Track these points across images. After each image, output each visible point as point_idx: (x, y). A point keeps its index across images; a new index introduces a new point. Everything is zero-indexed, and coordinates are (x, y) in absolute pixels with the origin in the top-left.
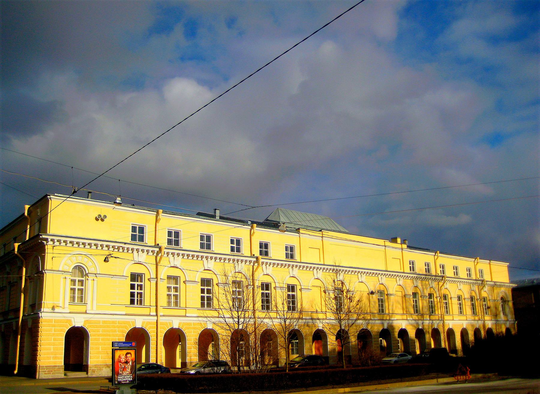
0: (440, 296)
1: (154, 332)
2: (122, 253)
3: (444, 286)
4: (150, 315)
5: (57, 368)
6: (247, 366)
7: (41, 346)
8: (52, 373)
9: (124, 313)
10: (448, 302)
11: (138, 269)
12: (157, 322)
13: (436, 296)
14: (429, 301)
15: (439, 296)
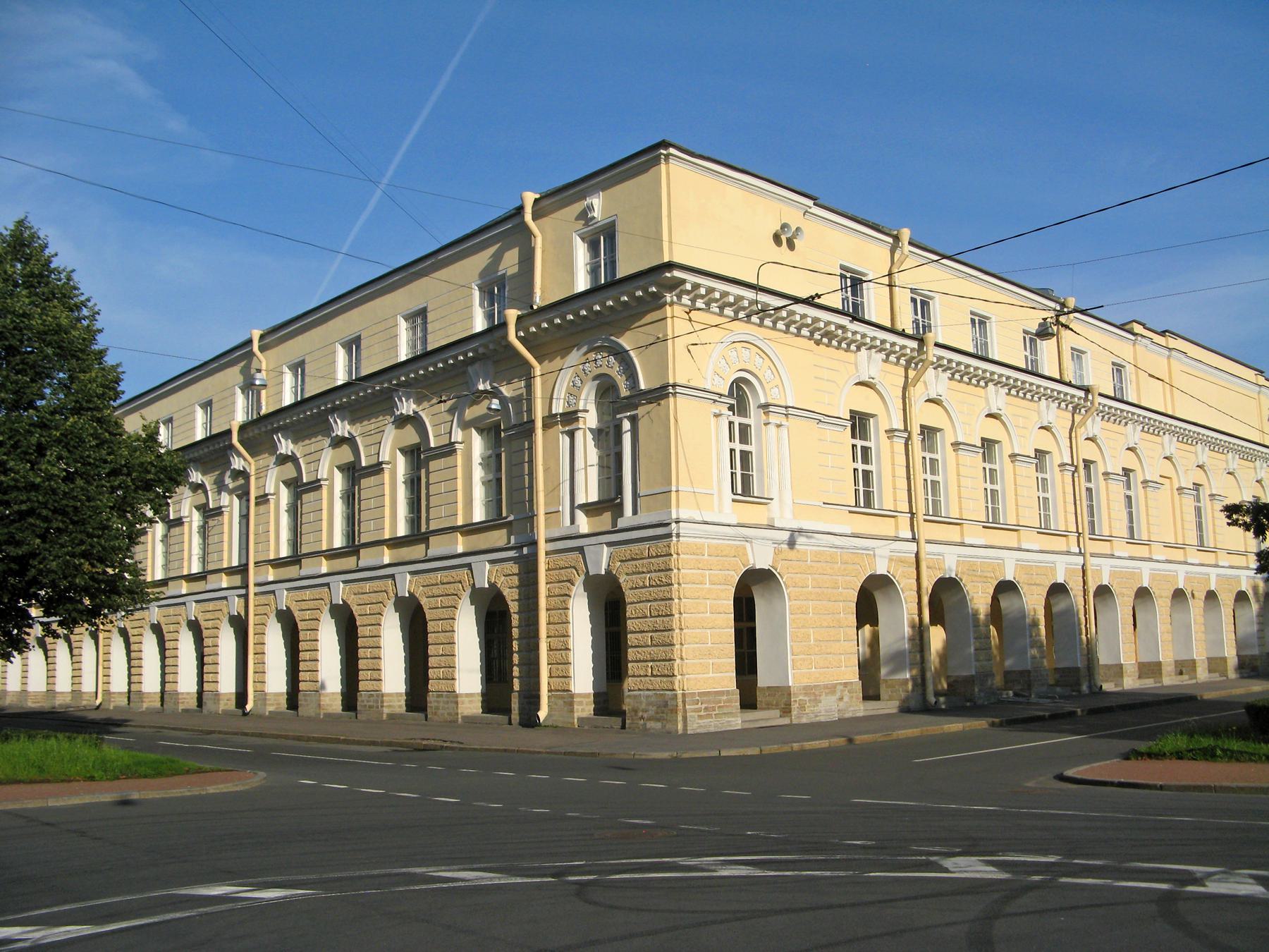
0: (1075, 464)
1: (911, 590)
2: (806, 340)
3: (1086, 429)
4: (897, 539)
5: (725, 698)
6: (685, 734)
7: (681, 629)
8: (715, 710)
9: (849, 532)
10: (1205, 505)
11: (865, 402)
12: (1084, 572)
13: (1142, 480)
14: (984, 468)
15: (1072, 465)
